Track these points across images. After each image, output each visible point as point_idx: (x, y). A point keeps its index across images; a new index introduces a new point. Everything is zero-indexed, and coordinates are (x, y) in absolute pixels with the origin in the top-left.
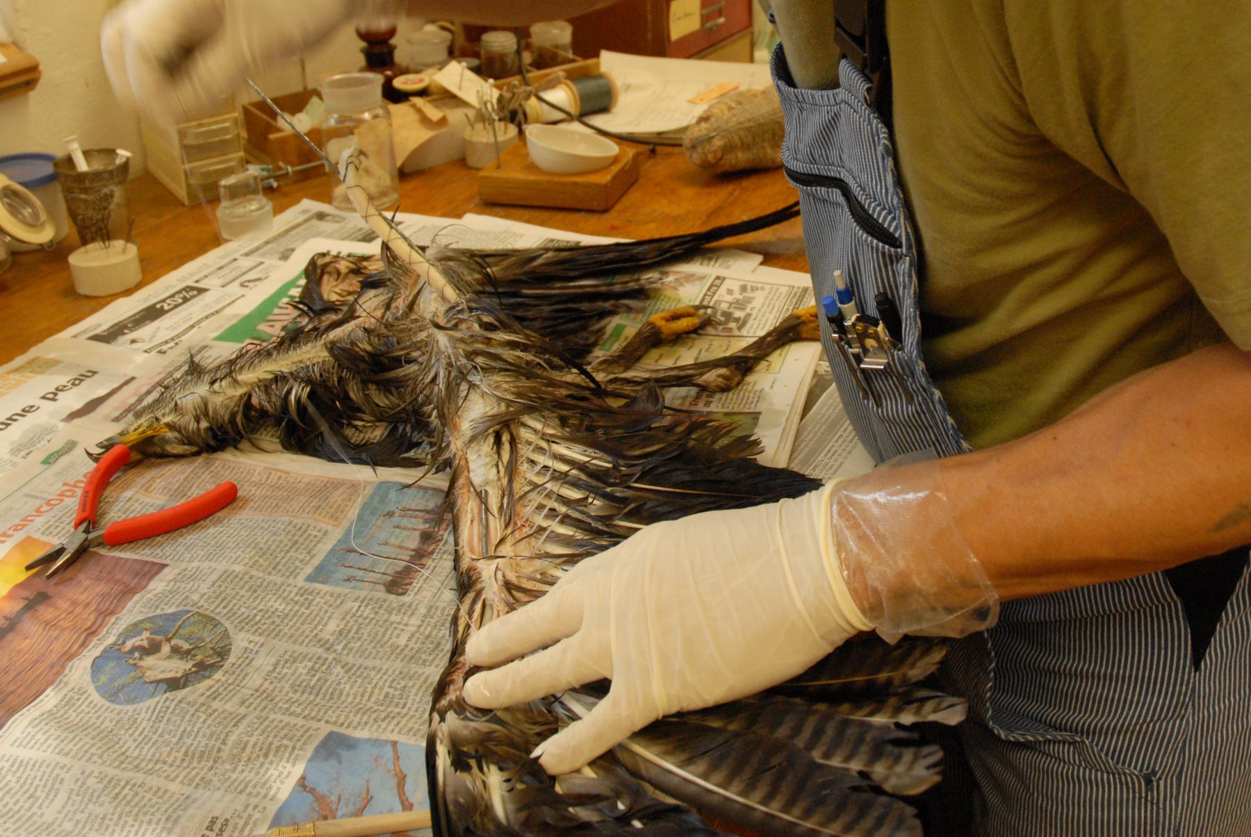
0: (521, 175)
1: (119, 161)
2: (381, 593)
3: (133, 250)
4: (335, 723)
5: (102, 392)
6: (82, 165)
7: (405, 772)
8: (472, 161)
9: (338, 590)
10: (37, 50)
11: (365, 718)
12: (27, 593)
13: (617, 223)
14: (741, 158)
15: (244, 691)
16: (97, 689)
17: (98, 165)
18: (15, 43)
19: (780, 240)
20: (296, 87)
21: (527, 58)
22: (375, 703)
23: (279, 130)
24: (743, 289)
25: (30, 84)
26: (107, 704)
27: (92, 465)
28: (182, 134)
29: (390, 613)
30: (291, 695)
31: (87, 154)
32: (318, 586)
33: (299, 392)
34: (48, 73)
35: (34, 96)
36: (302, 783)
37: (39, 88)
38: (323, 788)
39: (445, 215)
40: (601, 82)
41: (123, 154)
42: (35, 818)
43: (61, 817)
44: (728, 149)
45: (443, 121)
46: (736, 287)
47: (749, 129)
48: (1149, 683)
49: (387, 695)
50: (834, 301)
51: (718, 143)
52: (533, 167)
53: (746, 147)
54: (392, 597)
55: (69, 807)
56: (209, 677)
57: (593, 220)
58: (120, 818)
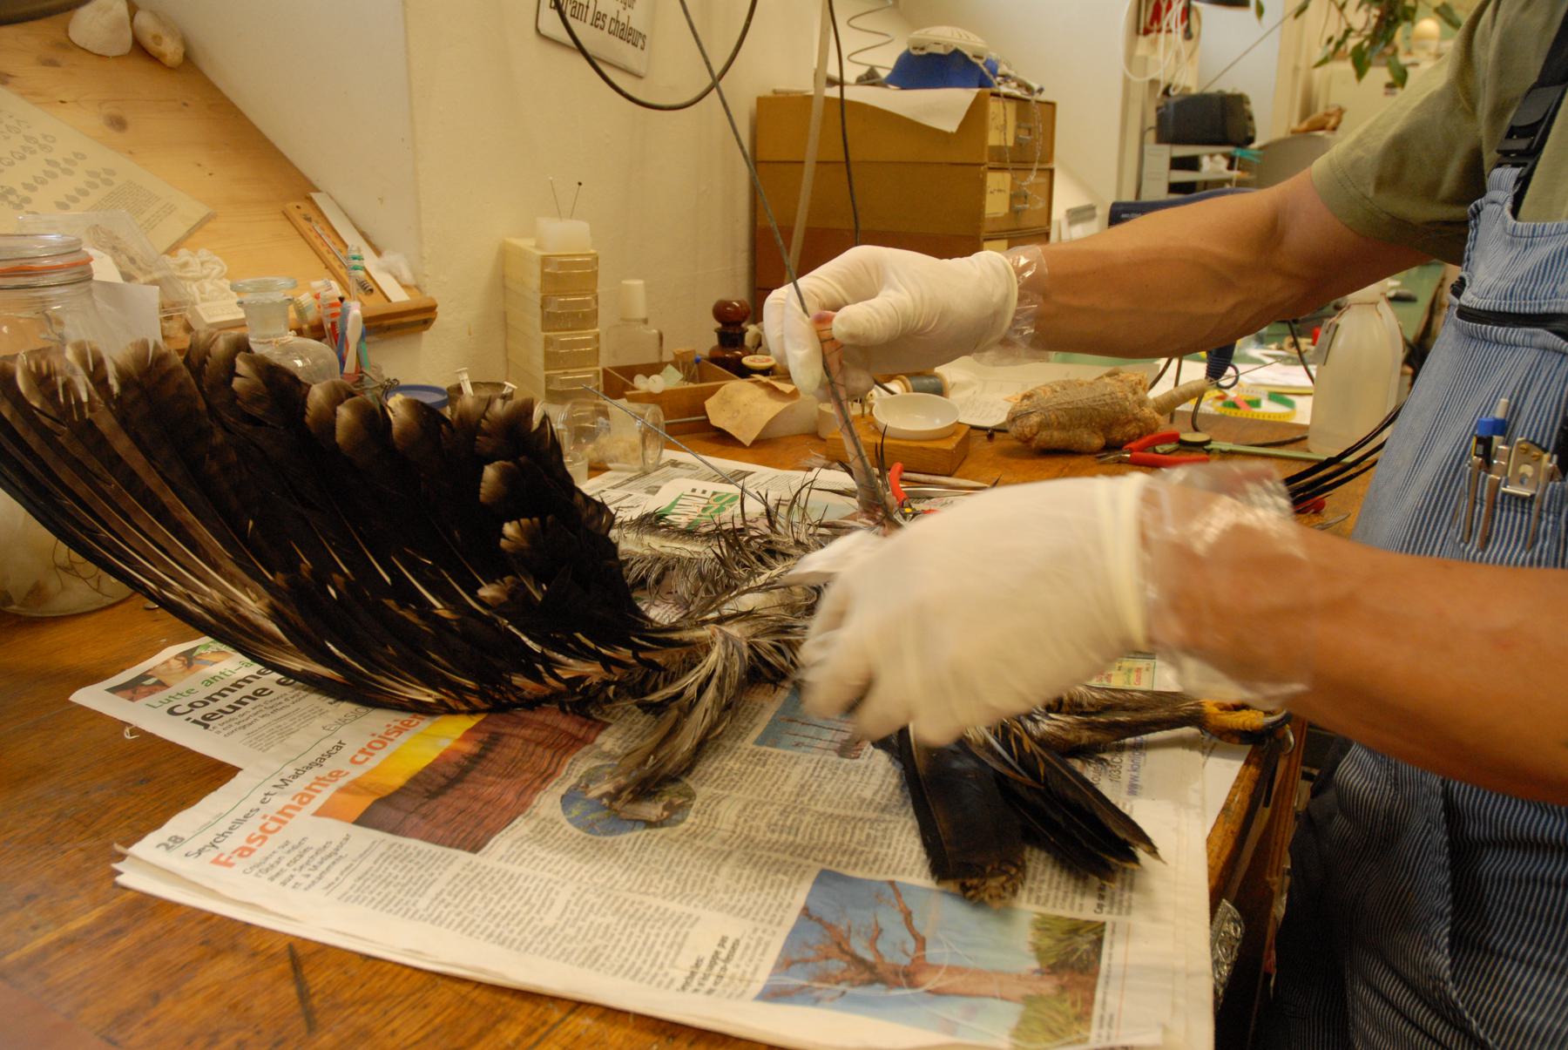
2: (834, 758)
4: (824, 861)
5: (271, 907)
7: (910, 908)
9: (789, 753)
10: (433, 293)
11: (854, 860)
12: (480, 736)
14: (1056, 437)
15: (720, 833)
16: (571, 821)
18: (417, 287)
19: (1359, 142)
20: (653, 359)
22: (859, 843)
25: (427, 323)
26: (583, 834)
28: (549, 379)
29: (848, 774)
30: (769, 835)
31: (474, 385)
32: (764, 748)
34: (442, 317)
35: (427, 335)
36: (806, 911)
38: (829, 917)
42: (535, 922)
43: (561, 923)
44: (1043, 425)
47: (1066, 410)
48: (1540, 996)
49: (868, 835)
51: (1035, 419)
53: (1062, 427)
54: (846, 761)
55: (567, 914)
56: (683, 821)
58: (625, 928)
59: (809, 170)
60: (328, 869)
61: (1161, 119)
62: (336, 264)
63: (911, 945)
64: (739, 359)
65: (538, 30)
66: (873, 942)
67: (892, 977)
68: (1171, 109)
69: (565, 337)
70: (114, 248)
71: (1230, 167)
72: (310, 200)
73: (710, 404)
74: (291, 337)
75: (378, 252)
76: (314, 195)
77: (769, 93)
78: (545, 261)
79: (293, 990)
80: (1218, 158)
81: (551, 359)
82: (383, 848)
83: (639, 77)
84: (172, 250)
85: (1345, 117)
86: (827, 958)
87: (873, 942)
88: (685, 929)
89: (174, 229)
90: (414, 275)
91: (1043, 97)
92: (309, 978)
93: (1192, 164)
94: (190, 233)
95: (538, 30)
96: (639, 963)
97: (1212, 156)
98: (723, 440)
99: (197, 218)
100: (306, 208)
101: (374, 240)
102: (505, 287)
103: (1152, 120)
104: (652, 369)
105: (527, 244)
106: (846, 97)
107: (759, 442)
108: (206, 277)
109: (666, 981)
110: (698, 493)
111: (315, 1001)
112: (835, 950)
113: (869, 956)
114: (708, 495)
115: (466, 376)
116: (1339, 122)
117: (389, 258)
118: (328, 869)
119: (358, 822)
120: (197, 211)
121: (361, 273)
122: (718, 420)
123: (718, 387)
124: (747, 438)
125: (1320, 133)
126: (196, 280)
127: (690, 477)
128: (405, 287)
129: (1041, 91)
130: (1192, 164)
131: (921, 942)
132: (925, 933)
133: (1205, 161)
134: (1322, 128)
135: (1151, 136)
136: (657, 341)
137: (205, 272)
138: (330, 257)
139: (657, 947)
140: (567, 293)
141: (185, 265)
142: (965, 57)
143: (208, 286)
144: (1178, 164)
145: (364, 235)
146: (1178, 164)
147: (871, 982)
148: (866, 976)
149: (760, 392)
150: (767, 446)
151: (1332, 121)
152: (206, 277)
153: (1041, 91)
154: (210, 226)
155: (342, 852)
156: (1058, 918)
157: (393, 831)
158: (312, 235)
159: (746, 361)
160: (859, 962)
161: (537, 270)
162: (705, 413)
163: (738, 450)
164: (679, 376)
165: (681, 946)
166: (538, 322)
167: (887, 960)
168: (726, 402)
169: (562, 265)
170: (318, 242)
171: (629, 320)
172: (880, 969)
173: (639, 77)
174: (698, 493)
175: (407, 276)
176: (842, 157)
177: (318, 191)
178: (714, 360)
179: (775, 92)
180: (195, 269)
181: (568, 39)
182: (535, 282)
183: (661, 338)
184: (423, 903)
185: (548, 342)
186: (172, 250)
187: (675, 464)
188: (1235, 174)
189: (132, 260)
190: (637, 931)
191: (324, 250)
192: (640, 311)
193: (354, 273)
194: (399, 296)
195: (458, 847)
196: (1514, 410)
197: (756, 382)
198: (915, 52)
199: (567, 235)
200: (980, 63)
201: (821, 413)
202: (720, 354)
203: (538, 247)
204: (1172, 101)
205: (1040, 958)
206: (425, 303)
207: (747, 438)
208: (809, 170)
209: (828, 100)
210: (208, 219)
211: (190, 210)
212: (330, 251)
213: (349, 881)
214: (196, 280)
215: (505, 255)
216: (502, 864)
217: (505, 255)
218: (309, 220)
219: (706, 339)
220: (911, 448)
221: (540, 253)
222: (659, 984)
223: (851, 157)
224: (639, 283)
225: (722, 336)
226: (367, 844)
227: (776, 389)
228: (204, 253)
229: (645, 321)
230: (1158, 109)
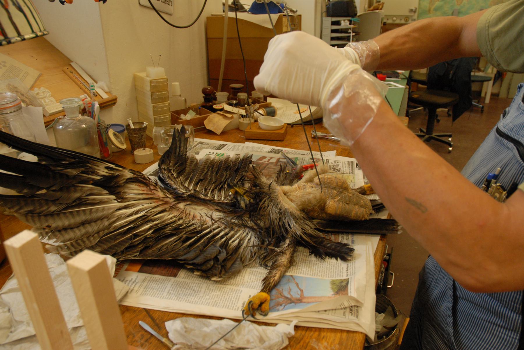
0: (259, 131)
1: (144, 126)
3: (152, 151)
6: (132, 127)
8: (241, 129)
10: (115, 94)
13: (287, 144)
17: (137, 127)
21: (250, 101)
23: (181, 119)
24: (335, 162)
25: (114, 104)
27: (49, 267)
28: (155, 119)
31: (133, 123)
33: (274, 161)
34: (119, 101)
35: (114, 108)
37: (116, 105)
39: (235, 142)
40: (272, 108)
41: (146, 124)
45: (232, 117)
46: (333, 162)
50: (233, 343)
52: (260, 128)
57: (279, 143)
59: (225, 41)
60: (135, 286)
61: (328, 9)
62: (84, 87)
63: (299, 292)
64: (212, 106)
65: (139, 3)
66: (289, 293)
67: (296, 301)
68: (331, 5)
69: (159, 105)
70: (16, 91)
71: (350, 24)
72: (70, 65)
73: (206, 122)
74: (80, 117)
75: (96, 82)
76: (71, 63)
77: (210, 15)
78: (151, 81)
79: (150, 319)
80: (346, 21)
81: (155, 113)
82: (149, 278)
83: (171, 15)
84: (32, 88)
85: (384, 5)
86: (278, 298)
87: (289, 293)
88: (239, 294)
89: (30, 81)
90: (108, 88)
91: (298, 13)
92: (153, 315)
93: (338, 23)
94: (36, 82)
95: (139, 3)
96: (228, 304)
97: (344, 20)
98: (210, 134)
99: (36, 76)
100: (70, 69)
101: (94, 77)
102: (136, 89)
103: (324, 9)
104: (185, 112)
105: (143, 75)
106: (238, 17)
107: (223, 133)
108: (45, 97)
109: (237, 308)
110: (211, 153)
111: (157, 321)
112: (280, 296)
113: (289, 296)
114: (215, 154)
115: (131, 121)
116: (382, 7)
117: (100, 83)
118: (135, 286)
119: (139, 272)
120: (36, 73)
121: (94, 91)
122: (209, 127)
123: (207, 117)
124: (219, 132)
125: (377, 11)
126: (42, 98)
127: (207, 148)
128: (106, 92)
129: (297, 11)
130: (338, 23)
131: (302, 291)
132: (302, 289)
133: (342, 22)
134: (377, 9)
135: (324, 14)
136: (184, 102)
137: (45, 95)
138: (81, 85)
139: (232, 299)
140: (159, 90)
141: (38, 94)
142: (274, 4)
143: (47, 101)
144: (333, 23)
145: (90, 76)
146: (333, 23)
147: (291, 303)
148: (289, 301)
149: (221, 117)
150: (225, 135)
151: (381, 7)
152: (45, 97)
153: (297, 11)
154: (41, 78)
155: (137, 281)
156: (337, 280)
157: (150, 273)
158: (74, 78)
159: (214, 107)
160: (287, 298)
161: (149, 84)
162: (204, 125)
163: (216, 137)
164: (194, 113)
165: (239, 299)
166: (150, 101)
167: (294, 297)
168: (210, 121)
169: (157, 82)
170: (76, 80)
171: (175, 96)
172: (293, 299)
173: (171, 15)
174: (211, 153)
175: (106, 89)
176: (237, 36)
177: (72, 62)
178: (203, 106)
179: (212, 15)
180: (41, 95)
181: (149, 5)
182: (148, 88)
183: (186, 100)
184: (165, 294)
185: (154, 107)
186: (32, 88)
187: (201, 143)
188: (352, 26)
189: (22, 95)
190: (226, 296)
191: (79, 83)
192: (179, 93)
193: (92, 91)
194: (105, 96)
195: (170, 276)
196: (501, 172)
197: (218, 114)
198: (258, 2)
199: (156, 72)
200: (278, 5)
201: (240, 122)
202: (205, 104)
203: (147, 76)
204: (331, 3)
205: (334, 291)
206: (114, 98)
207: (219, 132)
208: (225, 41)
209: (230, 18)
210: (40, 76)
211: (34, 73)
212: (81, 83)
213: (142, 289)
214: (42, 98)
215: (135, 78)
216: (184, 280)
217: (135, 78)
218: (72, 73)
219: (200, 99)
220: (272, 133)
221: (149, 79)
222: (235, 309)
223: (240, 37)
224: (177, 83)
225: (205, 98)
226: (144, 278)
227: (226, 116)
228: (42, 89)
229: (180, 96)
230: (326, 5)
